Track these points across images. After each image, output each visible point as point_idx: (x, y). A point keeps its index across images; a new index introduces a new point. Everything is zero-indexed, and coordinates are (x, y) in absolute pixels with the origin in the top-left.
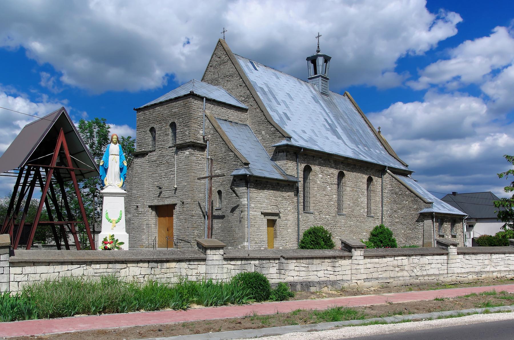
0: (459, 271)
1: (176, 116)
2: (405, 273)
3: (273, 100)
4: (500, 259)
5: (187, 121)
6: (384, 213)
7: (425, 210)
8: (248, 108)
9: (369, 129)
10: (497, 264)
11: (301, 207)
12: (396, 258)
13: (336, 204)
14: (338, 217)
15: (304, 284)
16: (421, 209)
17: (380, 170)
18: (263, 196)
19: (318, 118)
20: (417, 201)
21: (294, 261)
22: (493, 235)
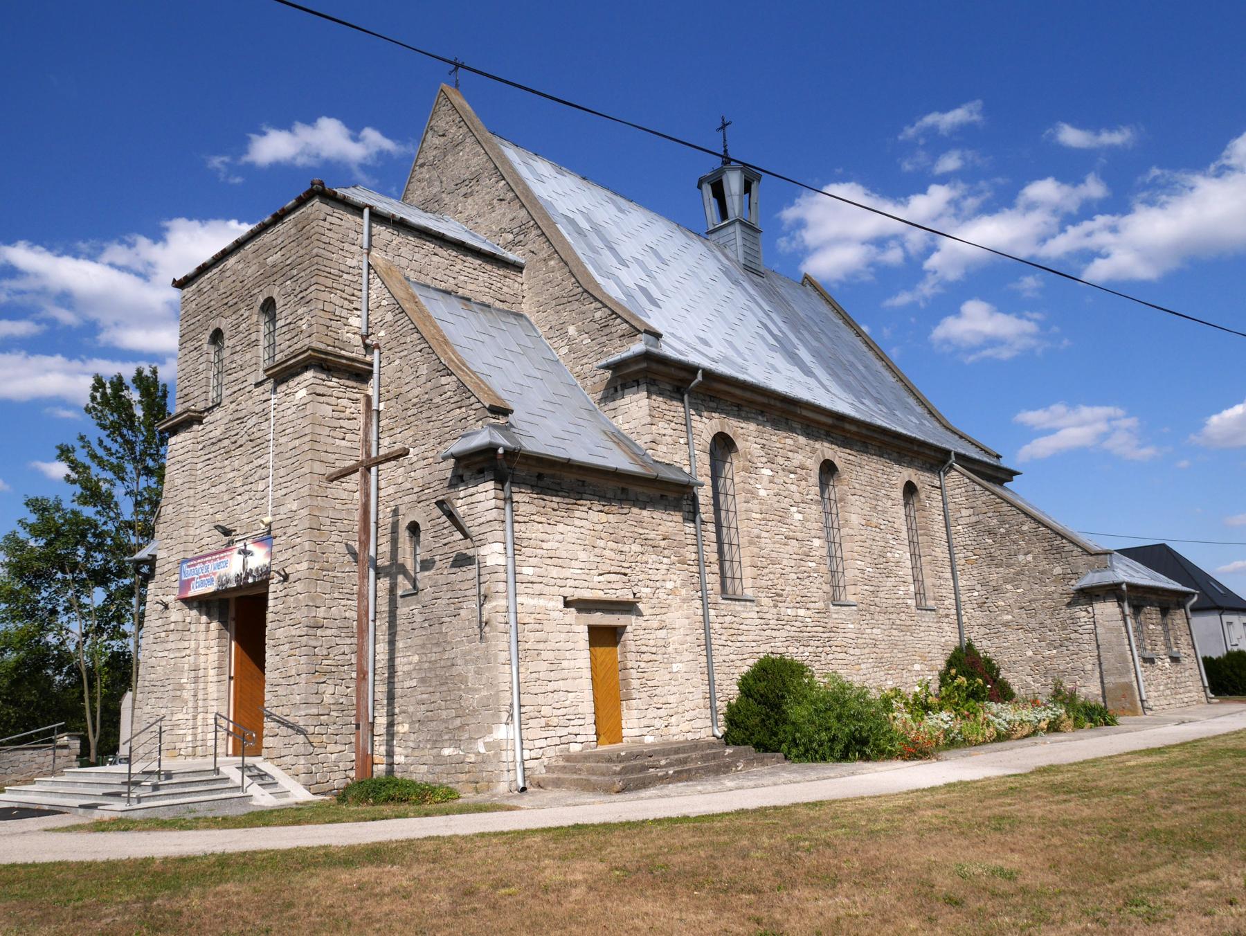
1: (275, 277)
5: (304, 286)
6: (963, 598)
7: (1091, 579)
9: (879, 365)
11: (713, 580)
14: (837, 614)
17: (935, 459)
18: (571, 537)
20: (1059, 550)
22: (1214, 657)
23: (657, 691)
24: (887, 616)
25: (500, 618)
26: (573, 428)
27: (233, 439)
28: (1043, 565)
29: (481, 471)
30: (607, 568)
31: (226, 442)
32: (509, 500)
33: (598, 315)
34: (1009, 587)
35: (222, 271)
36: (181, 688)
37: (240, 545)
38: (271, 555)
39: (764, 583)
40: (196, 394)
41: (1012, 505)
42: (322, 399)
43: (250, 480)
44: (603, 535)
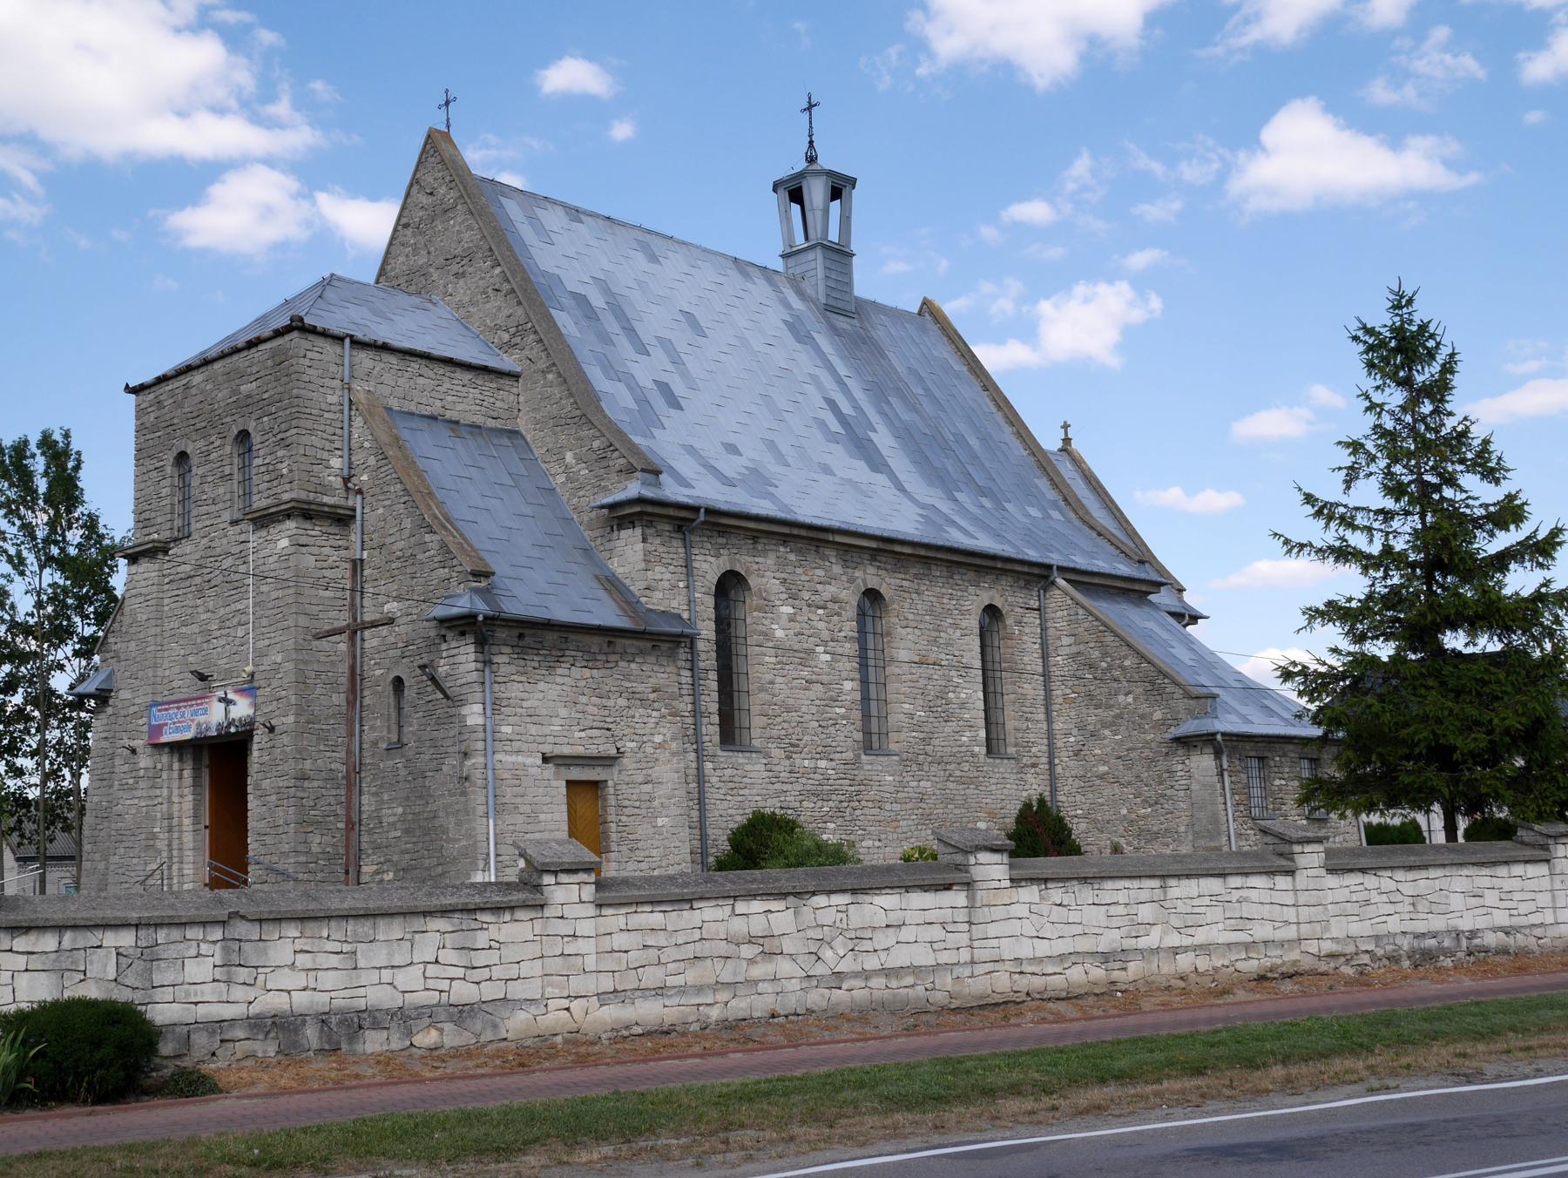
0: (1025, 950)
2: (784, 967)
3: (623, 342)
4: (1206, 901)
6: (1059, 744)
7: (1190, 727)
8: (519, 369)
10: (1190, 920)
11: (711, 731)
12: (741, 907)
13: (857, 715)
15: (334, 1020)
16: (1177, 721)
19: (800, 398)
21: (292, 931)
23: (639, 845)
24: (942, 766)
25: (478, 774)
26: (559, 578)
27: (207, 577)
28: (1144, 708)
29: (463, 634)
30: (589, 723)
31: (198, 580)
32: (488, 663)
33: (596, 444)
34: (1107, 732)
35: (187, 387)
36: (154, 836)
37: (221, 694)
38: (256, 706)
39: (775, 733)
40: (159, 520)
41: (1117, 635)
42: (304, 550)
43: (228, 624)
44: (586, 691)
